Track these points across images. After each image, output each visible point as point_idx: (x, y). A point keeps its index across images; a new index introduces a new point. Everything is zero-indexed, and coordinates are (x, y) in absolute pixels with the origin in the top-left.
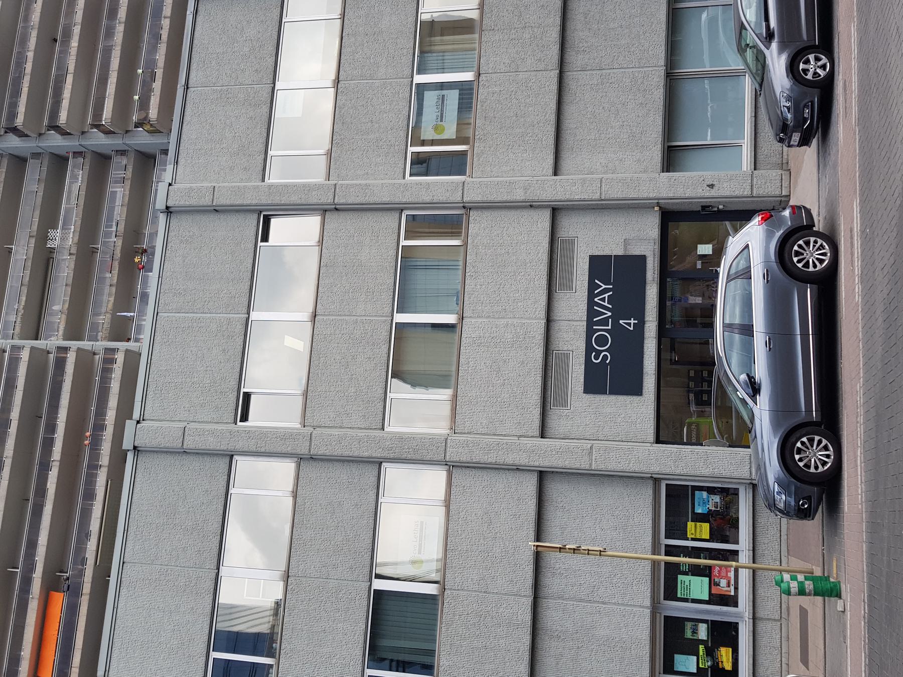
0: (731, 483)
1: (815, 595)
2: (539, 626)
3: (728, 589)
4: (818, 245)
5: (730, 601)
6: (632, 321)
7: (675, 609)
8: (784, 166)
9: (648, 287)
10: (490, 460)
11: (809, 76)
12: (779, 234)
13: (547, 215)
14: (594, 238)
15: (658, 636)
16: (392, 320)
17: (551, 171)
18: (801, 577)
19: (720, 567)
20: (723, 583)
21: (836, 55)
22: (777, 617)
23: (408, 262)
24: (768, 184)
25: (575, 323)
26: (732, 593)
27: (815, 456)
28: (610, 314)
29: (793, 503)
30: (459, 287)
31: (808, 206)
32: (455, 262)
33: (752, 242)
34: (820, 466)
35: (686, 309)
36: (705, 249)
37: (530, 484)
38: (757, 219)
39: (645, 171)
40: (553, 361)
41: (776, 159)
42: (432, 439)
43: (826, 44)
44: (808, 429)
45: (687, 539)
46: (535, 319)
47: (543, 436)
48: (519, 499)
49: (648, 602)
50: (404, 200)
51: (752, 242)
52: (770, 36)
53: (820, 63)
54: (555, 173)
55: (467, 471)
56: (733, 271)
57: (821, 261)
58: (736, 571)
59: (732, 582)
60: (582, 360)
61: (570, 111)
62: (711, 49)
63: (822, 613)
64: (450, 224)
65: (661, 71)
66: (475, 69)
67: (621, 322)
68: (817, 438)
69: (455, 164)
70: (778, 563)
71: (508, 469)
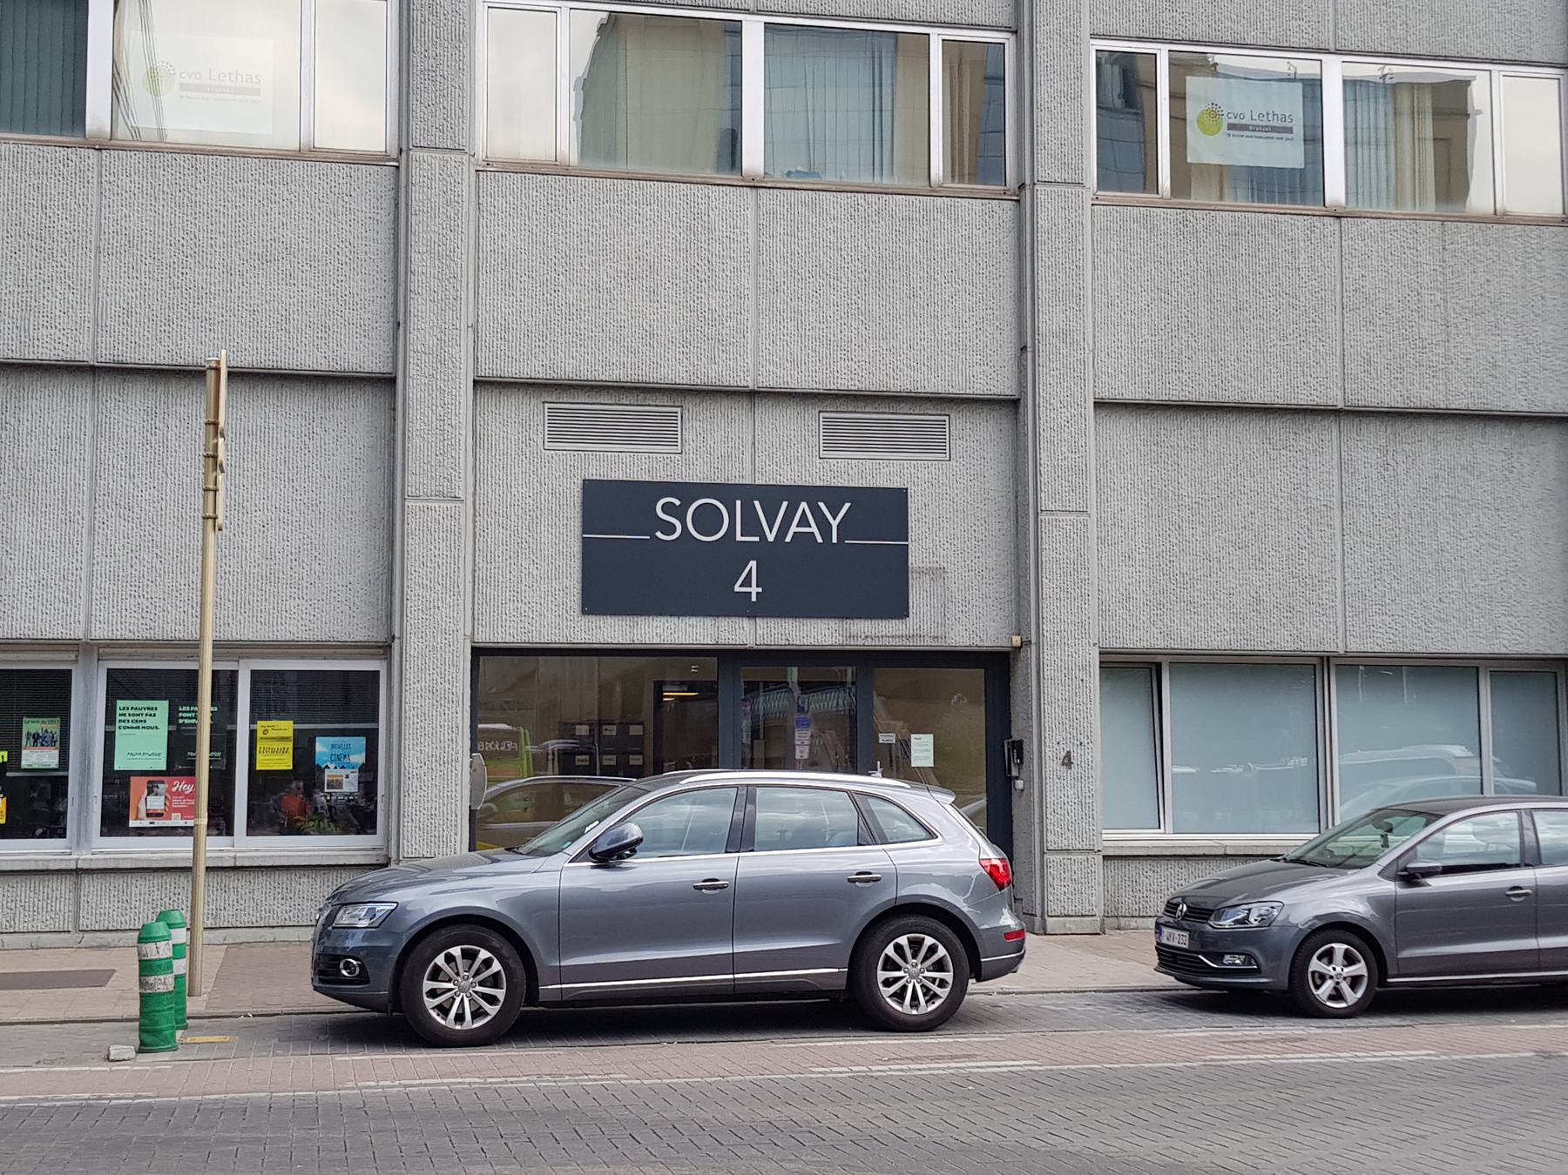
0: (388, 817)
1: (142, 995)
2: (26, 379)
3: (143, 813)
4: (935, 988)
5: (115, 821)
6: (754, 590)
7: (88, 695)
8: (1112, 921)
9: (833, 624)
10: (415, 257)
11: (1316, 965)
12: (961, 903)
13: (1003, 386)
14: (948, 502)
15: (22, 656)
16: (747, 11)
17: (1106, 394)
18: (181, 966)
19: (194, 795)
20: (156, 803)
21: (1364, 1021)
22: (84, 923)
23: (894, 50)
24: (1070, 886)
25: (747, 457)
26: (132, 823)
27: (460, 989)
28: (771, 537)
29: (350, 944)
30: (830, 178)
31: (1022, 967)
32: (887, 169)
33: (942, 847)
34: (437, 1001)
35: (781, 728)
36: (922, 750)
37: (365, 357)
38: (992, 855)
39: (1102, 612)
40: (657, 407)
41: (1128, 904)
42: (460, 112)
43: (1385, 1001)
44: (520, 974)
45: (253, 721)
46: (757, 364)
47: (478, 384)
48: (326, 328)
49: (100, 632)
50: (1039, 36)
51: (942, 847)
52: (1410, 878)
53: (1345, 986)
54: (1100, 405)
55: (387, 204)
56: (875, 805)
57: (899, 996)
58: (188, 831)
59: (158, 823)
60: (662, 476)
61: (1247, 436)
62: (1383, 753)
63: (100, 1016)
64: (983, 154)
65: (1333, 644)
66: (1352, 207)
67: (753, 564)
68: (500, 994)
69: (1126, 163)
70: (209, 923)
71: (395, 303)
